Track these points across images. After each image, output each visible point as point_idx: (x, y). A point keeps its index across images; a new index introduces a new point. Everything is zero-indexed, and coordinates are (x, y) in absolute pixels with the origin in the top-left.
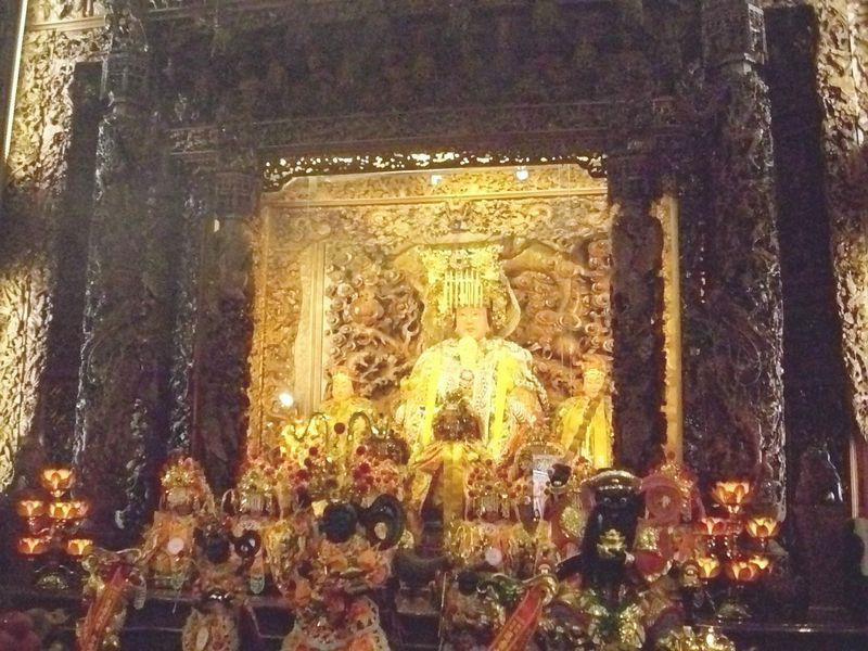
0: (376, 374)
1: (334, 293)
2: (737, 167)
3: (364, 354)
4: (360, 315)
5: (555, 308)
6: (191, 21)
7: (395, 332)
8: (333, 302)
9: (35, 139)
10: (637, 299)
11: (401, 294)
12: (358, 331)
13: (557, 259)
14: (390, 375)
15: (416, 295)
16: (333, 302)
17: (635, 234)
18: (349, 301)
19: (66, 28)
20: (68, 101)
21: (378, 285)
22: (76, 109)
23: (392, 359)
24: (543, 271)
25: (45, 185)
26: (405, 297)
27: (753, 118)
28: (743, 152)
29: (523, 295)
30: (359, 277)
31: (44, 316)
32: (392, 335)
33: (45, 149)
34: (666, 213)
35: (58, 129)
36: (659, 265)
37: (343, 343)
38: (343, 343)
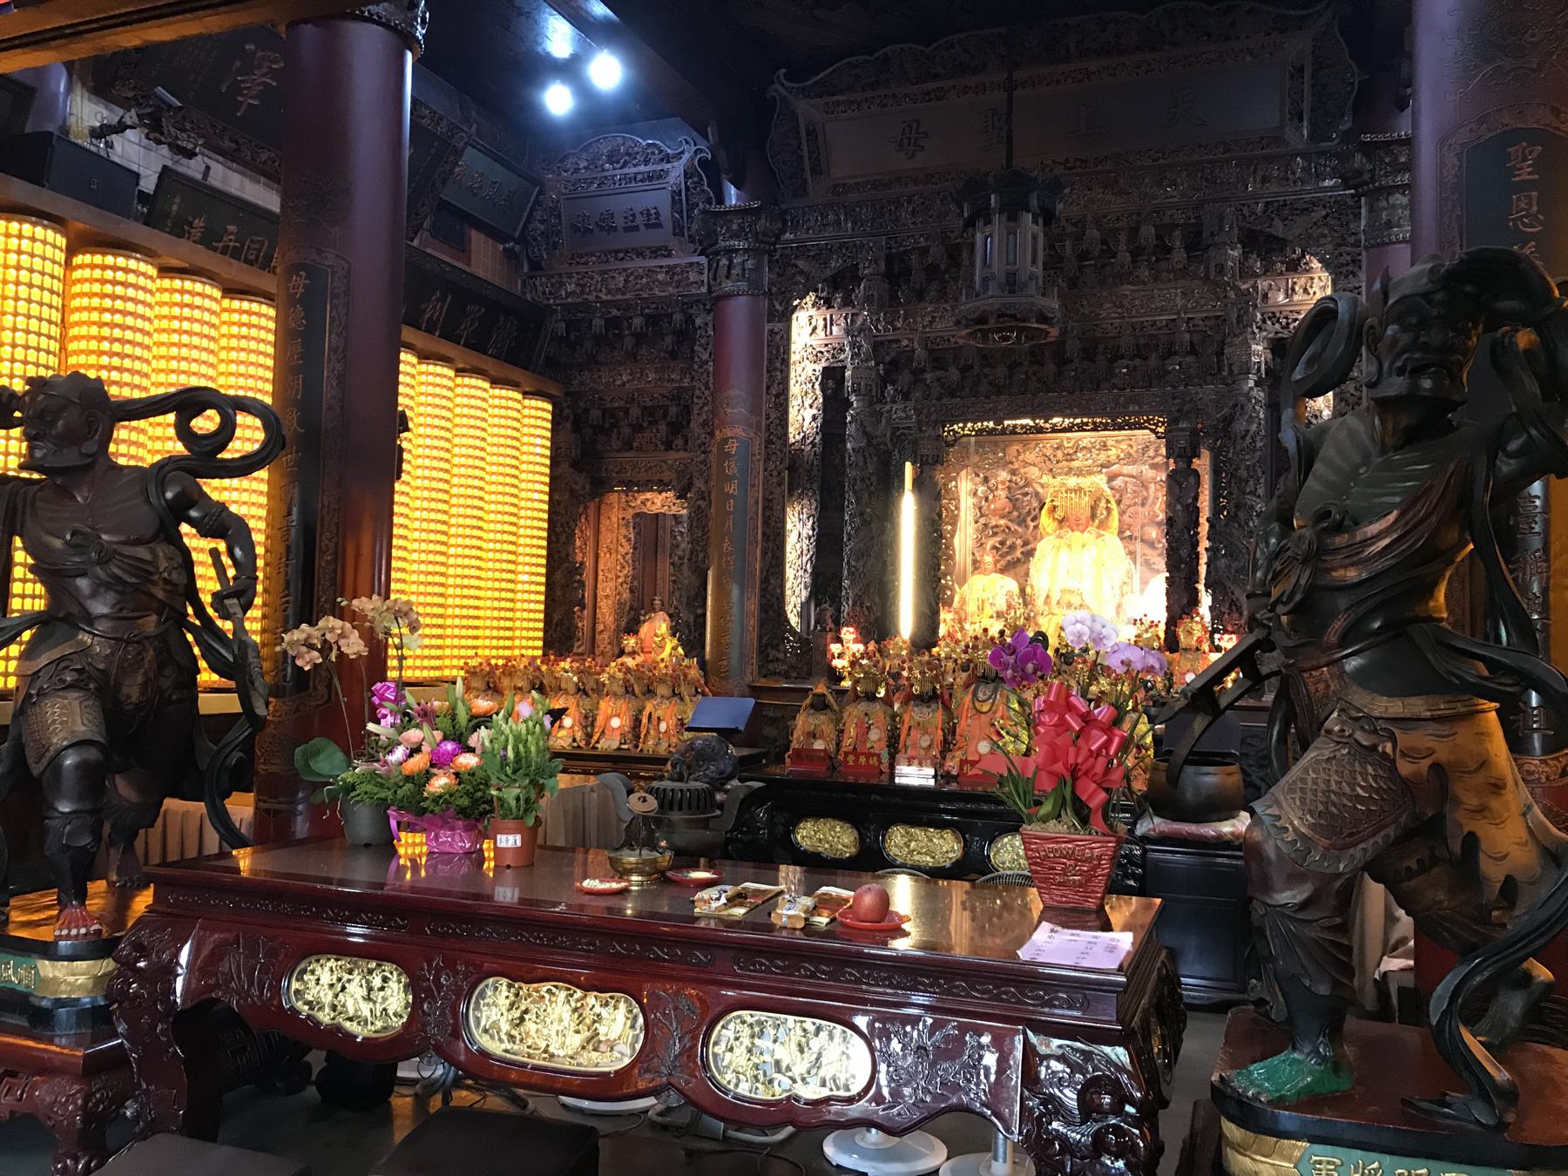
0: (1007, 553)
1: (975, 494)
2: (1238, 447)
3: (998, 539)
4: (995, 510)
5: (1143, 505)
6: (898, 341)
7: (1022, 522)
8: (975, 500)
9: (800, 418)
10: (1181, 520)
11: (1026, 494)
12: (993, 523)
13: (1145, 468)
14: (1018, 554)
15: (1037, 494)
16: (975, 500)
17: (1181, 485)
18: (987, 499)
19: (815, 343)
20: (818, 392)
21: (1009, 488)
22: (824, 397)
23: (1019, 542)
24: (1133, 477)
25: (809, 448)
26: (1028, 498)
27: (1251, 417)
28: (1243, 438)
29: (1118, 496)
30: (993, 481)
31: (813, 530)
32: (1019, 525)
33: (806, 424)
34: (1203, 464)
35: (815, 411)
36: (1196, 498)
37: (983, 531)
38: (983, 531)
